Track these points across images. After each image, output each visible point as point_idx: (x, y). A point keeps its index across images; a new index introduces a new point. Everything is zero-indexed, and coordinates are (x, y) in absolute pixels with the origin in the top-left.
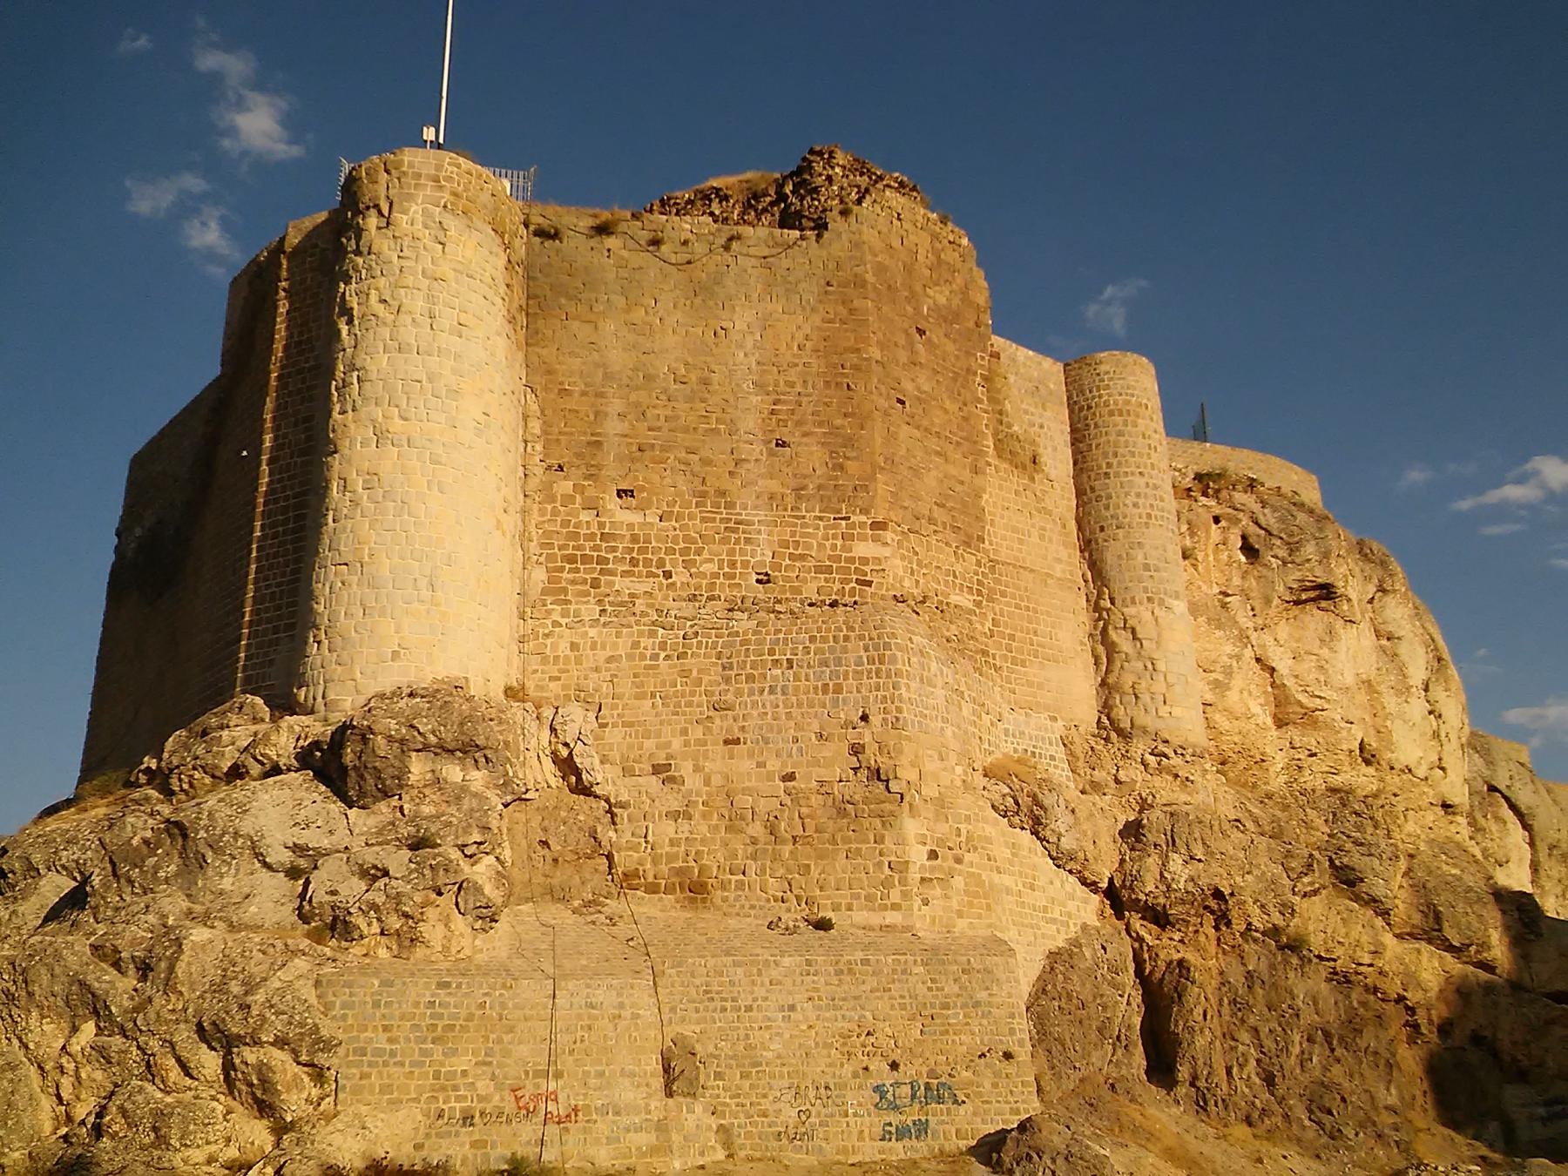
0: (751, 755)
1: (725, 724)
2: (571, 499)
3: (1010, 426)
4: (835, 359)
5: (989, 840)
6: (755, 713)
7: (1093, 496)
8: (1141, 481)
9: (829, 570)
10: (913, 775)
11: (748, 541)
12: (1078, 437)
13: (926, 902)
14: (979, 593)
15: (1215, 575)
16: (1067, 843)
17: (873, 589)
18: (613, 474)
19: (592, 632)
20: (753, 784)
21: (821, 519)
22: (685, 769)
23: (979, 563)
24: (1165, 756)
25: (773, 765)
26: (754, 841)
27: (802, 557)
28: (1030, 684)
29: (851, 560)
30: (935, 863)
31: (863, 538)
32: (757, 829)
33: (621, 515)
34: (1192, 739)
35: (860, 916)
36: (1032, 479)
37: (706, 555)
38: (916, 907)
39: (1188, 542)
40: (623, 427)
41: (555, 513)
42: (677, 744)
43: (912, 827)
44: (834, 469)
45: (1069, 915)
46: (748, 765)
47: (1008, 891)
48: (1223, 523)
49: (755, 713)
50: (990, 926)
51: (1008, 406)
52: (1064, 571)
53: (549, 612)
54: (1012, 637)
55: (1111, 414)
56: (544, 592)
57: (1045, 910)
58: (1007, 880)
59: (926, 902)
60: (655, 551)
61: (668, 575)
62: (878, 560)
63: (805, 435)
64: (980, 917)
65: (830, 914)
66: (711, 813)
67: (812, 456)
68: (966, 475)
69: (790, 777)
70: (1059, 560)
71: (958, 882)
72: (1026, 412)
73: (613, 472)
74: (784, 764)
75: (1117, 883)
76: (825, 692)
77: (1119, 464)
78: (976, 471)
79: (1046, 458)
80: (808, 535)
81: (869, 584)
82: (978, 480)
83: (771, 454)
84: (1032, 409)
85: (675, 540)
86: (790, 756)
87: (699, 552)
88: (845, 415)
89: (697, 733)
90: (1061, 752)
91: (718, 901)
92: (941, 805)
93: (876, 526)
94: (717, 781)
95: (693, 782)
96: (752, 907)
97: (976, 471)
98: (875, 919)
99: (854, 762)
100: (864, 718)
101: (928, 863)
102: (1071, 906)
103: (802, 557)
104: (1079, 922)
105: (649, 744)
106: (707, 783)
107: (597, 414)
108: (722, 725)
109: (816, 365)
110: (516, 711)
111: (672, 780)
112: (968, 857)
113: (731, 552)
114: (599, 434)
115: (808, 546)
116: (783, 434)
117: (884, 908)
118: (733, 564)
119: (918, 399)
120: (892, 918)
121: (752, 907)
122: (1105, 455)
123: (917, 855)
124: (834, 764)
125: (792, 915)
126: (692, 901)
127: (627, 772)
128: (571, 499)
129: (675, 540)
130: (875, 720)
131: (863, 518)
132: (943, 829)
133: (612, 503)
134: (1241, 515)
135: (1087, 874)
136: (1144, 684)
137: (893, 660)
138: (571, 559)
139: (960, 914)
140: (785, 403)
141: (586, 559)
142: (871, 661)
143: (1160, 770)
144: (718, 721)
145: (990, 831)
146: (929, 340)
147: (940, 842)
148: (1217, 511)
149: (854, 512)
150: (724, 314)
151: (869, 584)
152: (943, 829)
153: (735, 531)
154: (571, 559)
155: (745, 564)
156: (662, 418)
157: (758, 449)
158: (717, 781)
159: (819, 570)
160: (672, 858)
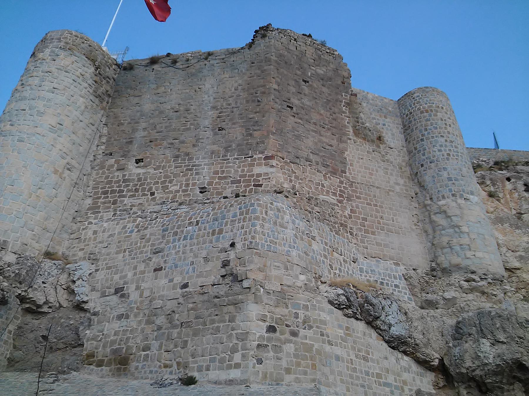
0: (166, 276)
1: (157, 260)
2: (112, 166)
3: (363, 123)
4: (252, 91)
5: (324, 323)
6: (173, 252)
7: (416, 151)
8: (443, 140)
9: (239, 182)
10: (260, 277)
11: (197, 174)
12: (407, 129)
13: (260, 362)
14: (341, 196)
15: (512, 205)
16: (396, 331)
17: (263, 188)
18: (135, 153)
19: (105, 225)
20: (165, 293)
21: (237, 159)
22: (131, 289)
23: (341, 182)
24: (474, 280)
25: (178, 280)
26: (159, 328)
27: (225, 178)
28: (378, 244)
29: (253, 176)
30: (271, 335)
31: (259, 165)
32: (161, 320)
33: (134, 170)
34: (492, 269)
35: (213, 375)
36: (379, 147)
37: (174, 182)
38: (251, 365)
39: (492, 189)
40: (143, 134)
41: (103, 173)
42: (130, 275)
43: (253, 310)
44: (247, 136)
45: (405, 383)
46: (163, 282)
47: (338, 358)
48: (513, 180)
49: (173, 252)
50: (314, 380)
51: (362, 115)
52: (402, 189)
53: (88, 218)
54: (365, 219)
55: (422, 112)
56: (89, 209)
57: (379, 376)
58: (338, 351)
59: (260, 362)
60: (148, 184)
61: (152, 194)
62: (267, 174)
63: (234, 124)
64: (305, 373)
65: (196, 374)
66: (139, 313)
67: (237, 133)
68: (334, 142)
69: (185, 286)
70: (398, 184)
71: (289, 348)
72: (374, 119)
73: (135, 151)
74: (183, 278)
75: (446, 362)
76: (213, 234)
77: (429, 133)
78: (340, 141)
79: (387, 137)
80: (230, 167)
81: (260, 186)
82: (342, 145)
83: (215, 134)
84: (377, 117)
85: (159, 178)
86: (188, 273)
87: (170, 182)
88: (256, 113)
89: (141, 267)
90: (403, 283)
91: (133, 370)
92: (283, 297)
93: (267, 158)
94: (146, 293)
95: (134, 296)
96: (151, 372)
97: (340, 141)
98: (223, 376)
99: (223, 272)
100: (233, 245)
101: (266, 335)
102: (406, 376)
103: (225, 178)
104: (415, 388)
105: (116, 277)
106: (141, 296)
107: (133, 130)
108: (156, 260)
109: (244, 95)
110: (48, 264)
111: (123, 296)
112: (302, 332)
113: (187, 180)
114: (132, 138)
115: (229, 172)
116: (223, 125)
117: (229, 367)
118: (187, 185)
119: (302, 108)
120: (234, 374)
121: (151, 372)
122: (421, 131)
123: (258, 330)
124: (212, 272)
125: (171, 376)
126: (119, 369)
127: (104, 295)
128: (112, 166)
129: (159, 178)
130: (238, 246)
131: (261, 156)
132: (281, 311)
133: (131, 166)
134: (522, 175)
135: (419, 355)
136: (455, 240)
137: (254, 211)
138: (105, 193)
139: (288, 371)
140: (225, 112)
141: (113, 192)
142: (241, 214)
143: (472, 290)
144: (154, 260)
145: (324, 316)
146: (311, 86)
147: (279, 321)
148: (508, 175)
149: (256, 154)
150: (200, 83)
151: (260, 186)
152: (281, 311)
153: (191, 170)
154: (105, 193)
155: (194, 184)
156: (164, 127)
157: (209, 133)
158: (146, 293)
159: (233, 182)
160: (113, 342)
